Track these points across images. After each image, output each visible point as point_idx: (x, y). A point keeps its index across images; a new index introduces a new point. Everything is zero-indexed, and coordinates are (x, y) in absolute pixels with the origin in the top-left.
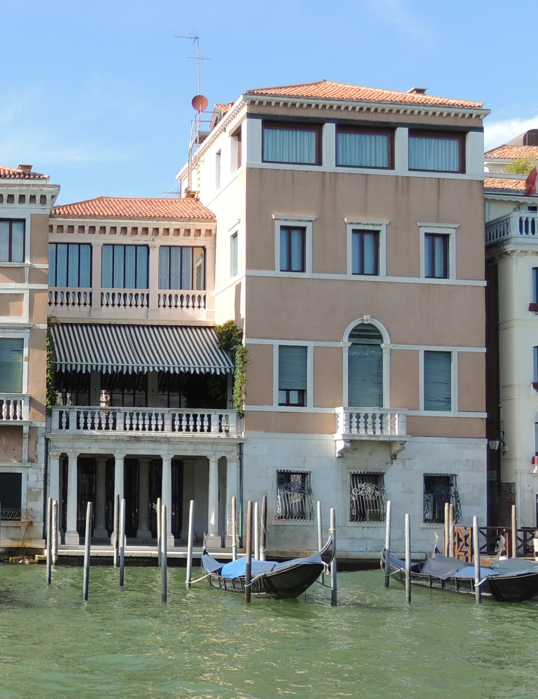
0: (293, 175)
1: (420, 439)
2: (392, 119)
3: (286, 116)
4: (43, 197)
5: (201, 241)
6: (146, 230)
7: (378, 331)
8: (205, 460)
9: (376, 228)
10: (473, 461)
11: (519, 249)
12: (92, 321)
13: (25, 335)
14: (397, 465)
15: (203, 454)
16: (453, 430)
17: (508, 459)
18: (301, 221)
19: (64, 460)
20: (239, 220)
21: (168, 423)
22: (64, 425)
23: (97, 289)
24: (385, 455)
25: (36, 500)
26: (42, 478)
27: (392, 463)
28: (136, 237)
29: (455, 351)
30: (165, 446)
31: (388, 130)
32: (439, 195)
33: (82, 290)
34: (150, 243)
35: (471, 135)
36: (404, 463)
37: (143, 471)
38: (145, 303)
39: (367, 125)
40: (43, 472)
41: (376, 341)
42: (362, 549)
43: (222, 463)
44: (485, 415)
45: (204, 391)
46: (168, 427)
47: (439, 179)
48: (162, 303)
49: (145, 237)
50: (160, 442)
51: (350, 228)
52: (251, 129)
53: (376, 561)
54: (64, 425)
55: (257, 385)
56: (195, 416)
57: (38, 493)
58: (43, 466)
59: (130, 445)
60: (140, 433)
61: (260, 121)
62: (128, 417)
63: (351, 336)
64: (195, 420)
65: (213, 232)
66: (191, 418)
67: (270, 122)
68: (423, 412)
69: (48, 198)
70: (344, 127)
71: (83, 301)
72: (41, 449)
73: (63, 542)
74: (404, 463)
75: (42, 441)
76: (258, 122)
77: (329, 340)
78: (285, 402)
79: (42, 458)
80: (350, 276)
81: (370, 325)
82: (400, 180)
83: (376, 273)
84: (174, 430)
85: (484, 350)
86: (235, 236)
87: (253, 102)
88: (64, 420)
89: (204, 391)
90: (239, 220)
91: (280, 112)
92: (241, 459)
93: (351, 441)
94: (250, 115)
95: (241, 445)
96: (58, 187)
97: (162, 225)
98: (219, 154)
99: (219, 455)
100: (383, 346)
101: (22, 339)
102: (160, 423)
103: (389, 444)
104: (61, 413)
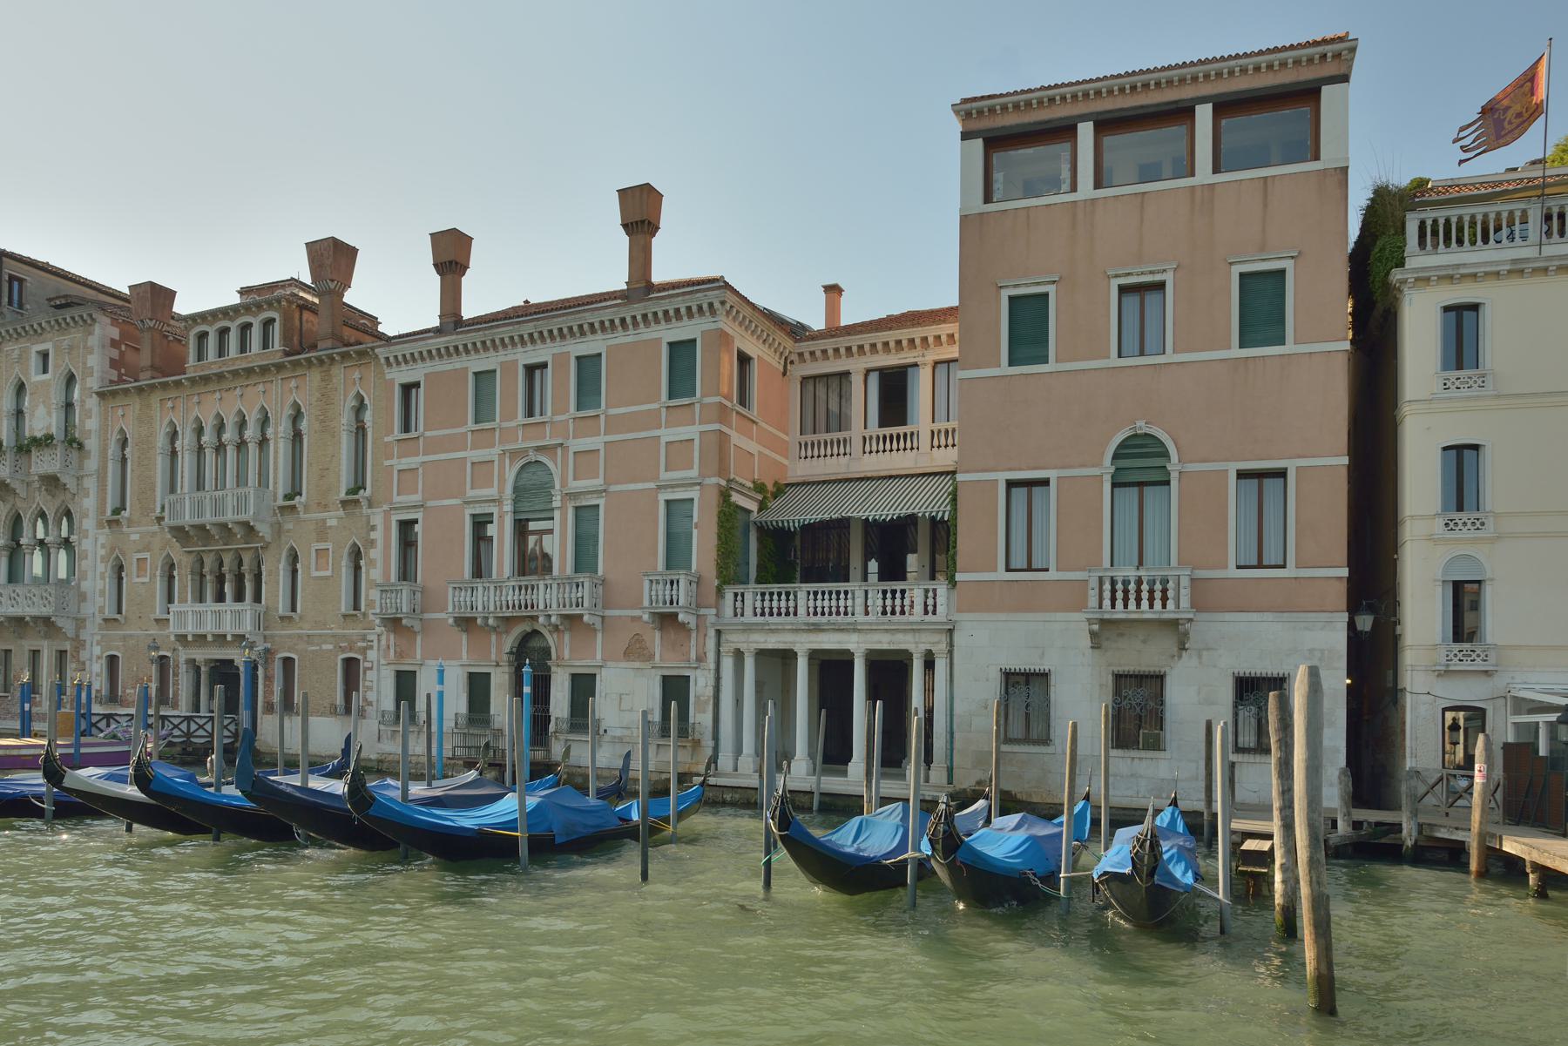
1: (1228, 616)
2: (1187, 93)
9: (1158, 278)
10: (1322, 651)
11: (1411, 277)
13: (694, 493)
14: (1188, 662)
15: (903, 647)
22: (930, 608)
24: (1168, 643)
26: (711, 682)
27: (1180, 657)
28: (902, 355)
30: (854, 637)
31: (1182, 113)
32: (1265, 205)
34: (919, 360)
36: (1200, 657)
42: (1130, 793)
44: (1345, 572)
47: (1265, 178)
54: (930, 608)
56: (894, 592)
57: (706, 702)
58: (712, 666)
63: (1116, 457)
74: (1200, 657)
75: (712, 633)
76: (978, 144)
79: (711, 656)
80: (1114, 361)
85: (1345, 460)
88: (930, 602)
91: (1011, 120)
92: (951, 652)
95: (951, 631)
99: (923, 647)
103: (1175, 623)
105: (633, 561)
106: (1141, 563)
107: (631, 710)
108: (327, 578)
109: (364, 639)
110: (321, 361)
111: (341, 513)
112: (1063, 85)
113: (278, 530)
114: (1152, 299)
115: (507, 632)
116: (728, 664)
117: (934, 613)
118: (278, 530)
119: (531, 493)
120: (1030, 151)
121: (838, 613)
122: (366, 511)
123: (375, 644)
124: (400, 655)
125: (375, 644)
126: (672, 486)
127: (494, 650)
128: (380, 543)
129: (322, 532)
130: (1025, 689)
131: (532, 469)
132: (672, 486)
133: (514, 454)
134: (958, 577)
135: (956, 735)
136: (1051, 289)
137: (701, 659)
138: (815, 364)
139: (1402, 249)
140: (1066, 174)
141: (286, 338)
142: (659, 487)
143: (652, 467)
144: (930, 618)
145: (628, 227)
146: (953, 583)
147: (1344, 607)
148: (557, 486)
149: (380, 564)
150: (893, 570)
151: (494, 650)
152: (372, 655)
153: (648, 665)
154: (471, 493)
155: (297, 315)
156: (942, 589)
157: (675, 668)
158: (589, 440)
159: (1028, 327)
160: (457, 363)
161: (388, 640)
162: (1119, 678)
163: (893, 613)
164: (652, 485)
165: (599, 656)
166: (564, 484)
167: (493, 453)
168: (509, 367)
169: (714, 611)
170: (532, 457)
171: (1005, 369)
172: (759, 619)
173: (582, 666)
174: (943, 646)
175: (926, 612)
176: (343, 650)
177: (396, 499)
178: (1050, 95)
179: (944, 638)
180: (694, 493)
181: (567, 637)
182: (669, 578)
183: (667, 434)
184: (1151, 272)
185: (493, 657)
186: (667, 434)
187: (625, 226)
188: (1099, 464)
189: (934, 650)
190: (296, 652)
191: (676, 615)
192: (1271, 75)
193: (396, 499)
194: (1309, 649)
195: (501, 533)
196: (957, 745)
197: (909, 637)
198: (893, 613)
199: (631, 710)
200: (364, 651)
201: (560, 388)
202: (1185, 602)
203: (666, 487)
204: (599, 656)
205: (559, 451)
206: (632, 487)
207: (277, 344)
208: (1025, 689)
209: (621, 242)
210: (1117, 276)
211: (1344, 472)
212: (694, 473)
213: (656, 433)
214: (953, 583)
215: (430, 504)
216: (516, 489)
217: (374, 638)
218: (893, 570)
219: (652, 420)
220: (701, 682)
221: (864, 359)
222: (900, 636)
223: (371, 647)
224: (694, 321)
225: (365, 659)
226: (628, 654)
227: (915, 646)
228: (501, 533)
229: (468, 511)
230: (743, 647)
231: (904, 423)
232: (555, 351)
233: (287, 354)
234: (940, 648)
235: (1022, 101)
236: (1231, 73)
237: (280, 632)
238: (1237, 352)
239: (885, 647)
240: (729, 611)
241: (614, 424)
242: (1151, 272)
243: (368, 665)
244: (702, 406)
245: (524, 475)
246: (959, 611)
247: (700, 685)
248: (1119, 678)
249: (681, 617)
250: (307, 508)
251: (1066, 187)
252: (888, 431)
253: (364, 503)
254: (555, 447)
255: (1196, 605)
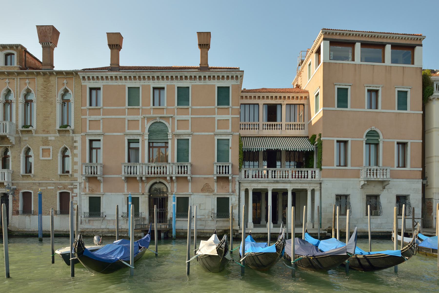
0: (343, 66)
1: (395, 180)
2: (384, 41)
3: (340, 39)
4: (237, 77)
5: (302, 102)
6: (280, 97)
7: (377, 133)
8: (305, 191)
9: (377, 89)
12: (259, 136)
13: (230, 137)
14: (385, 191)
15: (305, 188)
16: (408, 176)
17: (430, 188)
18: (346, 85)
19: (247, 191)
20: (320, 87)
21: (290, 174)
22: (313, 176)
23: (261, 123)
24: (380, 187)
25: (235, 209)
26: (237, 199)
28: (277, 101)
29: (409, 142)
30: (289, 185)
32: (403, 74)
33: (255, 123)
34: (282, 103)
35: (417, 48)
36: (388, 190)
37: (279, 196)
38: (280, 128)
39: (374, 45)
40: (238, 197)
41: (377, 138)
43: (313, 191)
45: (305, 159)
46: (290, 176)
48: (287, 128)
49: (280, 101)
50: (287, 183)
51: (366, 89)
52: (324, 46)
53: (388, 234)
55: (330, 154)
58: (238, 194)
59: (274, 185)
60: (279, 179)
61: (329, 42)
62: (273, 172)
63: (366, 136)
64: (301, 173)
65: (307, 97)
66: (300, 172)
67: (333, 43)
68: (396, 169)
69: (239, 77)
70: (364, 45)
71: (255, 128)
72: (237, 187)
73: (247, 227)
74: (388, 190)
75: (238, 183)
77: (358, 138)
78: (338, 165)
79: (237, 191)
81: (374, 131)
82: (387, 67)
83: (377, 108)
84: (293, 178)
86: (318, 94)
87: (326, 33)
89: (305, 159)
90: (320, 87)
91: (338, 37)
92: (321, 190)
93: (367, 181)
94: (324, 39)
95: (321, 183)
96: (243, 71)
97: (287, 95)
98: (310, 65)
99: (312, 188)
100: (379, 140)
101: (229, 139)
102: (287, 174)
103: (382, 182)
104: (245, 171)
105: (203, 157)
106: (370, 165)
107: (205, 209)
108: (49, 160)
109: (72, 184)
110: (45, 74)
111: (58, 135)
112: (337, 30)
113: (19, 140)
114: (162, 91)
115: (147, 183)
116: (243, 194)
117: (315, 178)
118: (19, 140)
119: (158, 134)
120: (340, 47)
121: (283, 177)
122: (71, 135)
123: (78, 187)
124: (92, 191)
125: (78, 187)
126: (221, 135)
127: (140, 189)
128: (79, 148)
129: (46, 142)
130: (342, 200)
131: (157, 124)
132: (221, 135)
133: (149, 119)
134: (323, 167)
135: (323, 214)
136: (349, 87)
137: (233, 192)
138: (246, 100)
139: (433, 90)
140: (350, 56)
141: (20, 62)
142: (215, 135)
143: (208, 128)
144: (313, 179)
145: (200, 45)
146: (321, 169)
147: (421, 178)
148: (170, 131)
149: (79, 155)
150: (272, 164)
151: (140, 189)
152: (76, 191)
153: (212, 194)
154: (127, 131)
155: (24, 54)
156: (317, 171)
157: (223, 194)
158: (184, 116)
159: (342, 97)
160: (120, 83)
161: (85, 185)
162: (367, 196)
163: (301, 177)
164: (212, 134)
165: (190, 191)
166: (173, 130)
167: (139, 117)
168: (171, 87)
169: (238, 176)
170: (158, 120)
171: (336, 108)
172: (254, 179)
173: (182, 194)
174: (318, 188)
175: (312, 178)
176: (60, 189)
177: (88, 131)
178: (350, 33)
179: (319, 186)
180: (230, 137)
181: (175, 185)
182: (218, 165)
183: (218, 117)
184: (376, 87)
185: (140, 191)
186: (218, 117)
187: (109, 45)
188: (362, 138)
189: (315, 189)
190: (32, 190)
191: (97, 177)
192: (405, 41)
193: (88, 131)
194: (412, 189)
195: (143, 147)
196: (323, 216)
197: (307, 185)
198: (301, 177)
199: (205, 209)
200: (72, 189)
201: (169, 98)
202: (388, 176)
203: (218, 135)
204: (190, 191)
205: (170, 119)
206: (203, 133)
207: (15, 63)
208: (342, 200)
209: (198, 51)
210: (367, 86)
211: (421, 144)
212: (230, 130)
213: (214, 116)
214: (321, 169)
215: (106, 134)
216: (149, 131)
217: (78, 184)
218: (272, 164)
219: (212, 112)
220: (234, 199)
221: (263, 100)
222: (304, 185)
223: (76, 188)
224: (228, 81)
225: (73, 192)
226: (203, 190)
227: (309, 188)
228: (143, 147)
229: (216, 138)
230: (249, 188)
231: (276, 121)
232: (169, 84)
233: (21, 69)
234: (317, 188)
235: (372, 34)
236: (384, 37)
237: (22, 182)
238: (397, 111)
239: (299, 188)
240: (243, 176)
241: (194, 112)
242: (376, 87)
243: (73, 195)
244: (232, 109)
245: (153, 126)
246: (323, 177)
247: (233, 200)
248: (367, 196)
249: (98, 178)
250: (36, 132)
251: (350, 59)
252: (269, 123)
253: (71, 132)
254: (169, 117)
255: (392, 177)
